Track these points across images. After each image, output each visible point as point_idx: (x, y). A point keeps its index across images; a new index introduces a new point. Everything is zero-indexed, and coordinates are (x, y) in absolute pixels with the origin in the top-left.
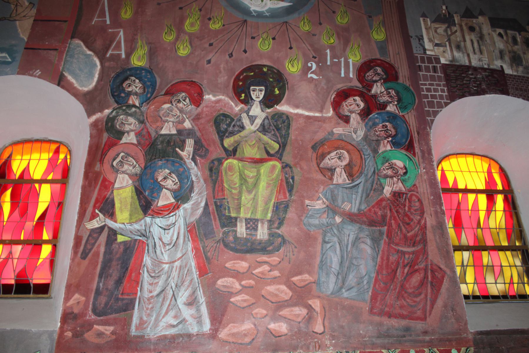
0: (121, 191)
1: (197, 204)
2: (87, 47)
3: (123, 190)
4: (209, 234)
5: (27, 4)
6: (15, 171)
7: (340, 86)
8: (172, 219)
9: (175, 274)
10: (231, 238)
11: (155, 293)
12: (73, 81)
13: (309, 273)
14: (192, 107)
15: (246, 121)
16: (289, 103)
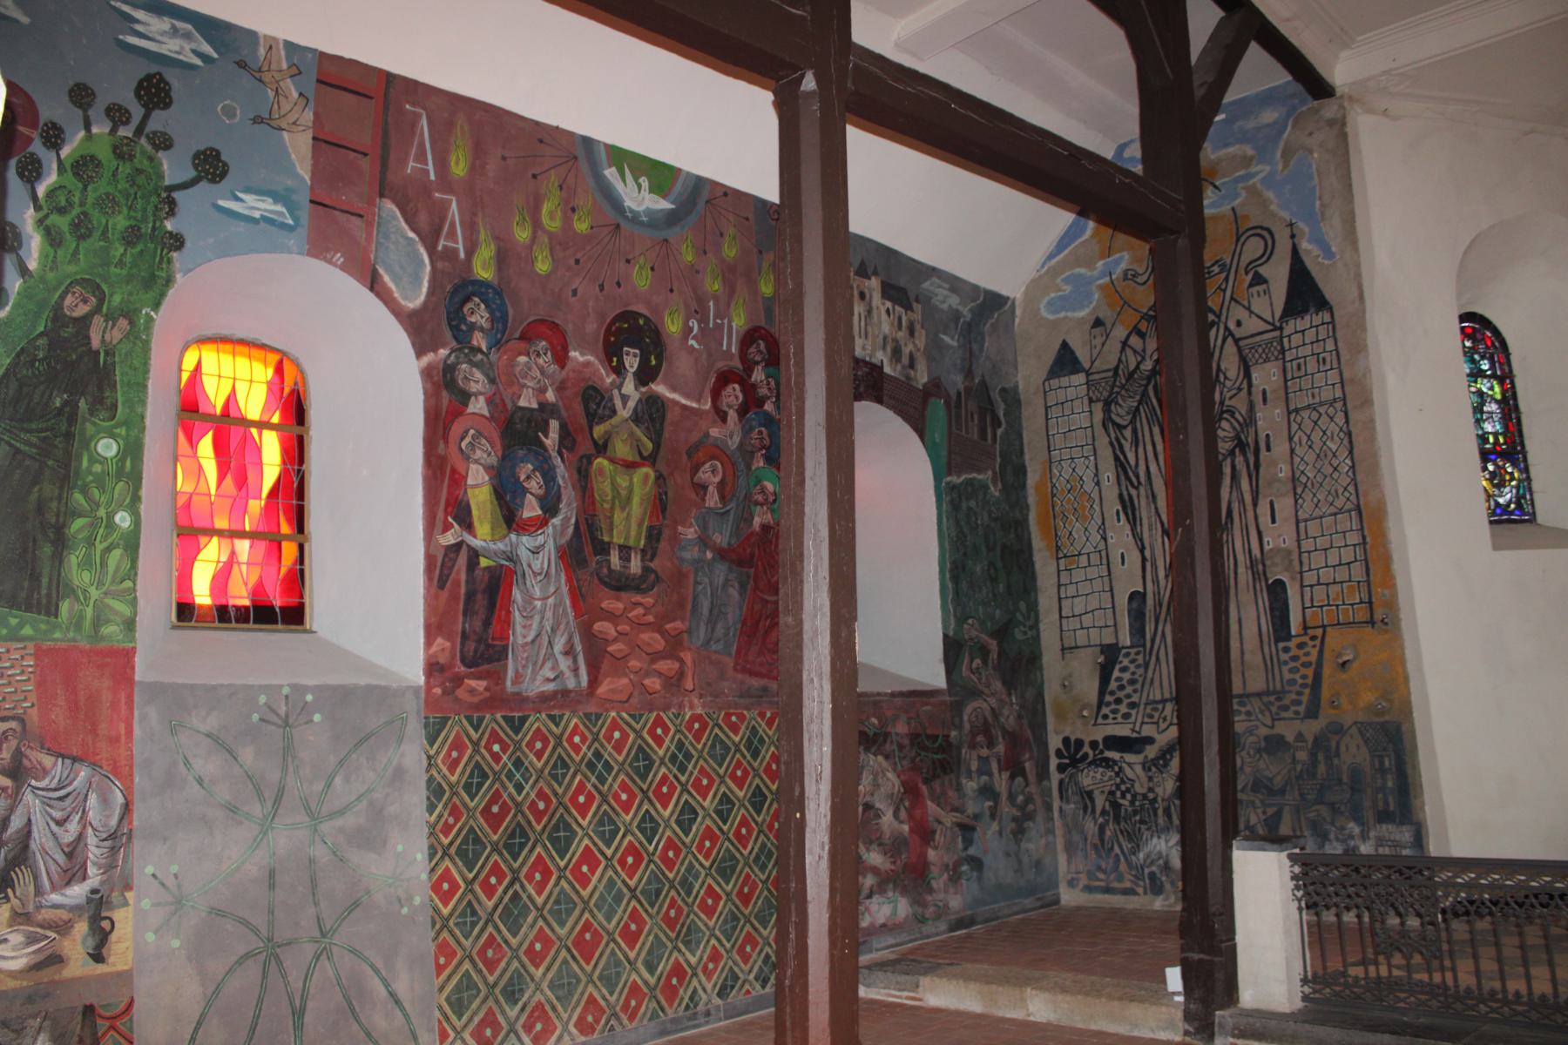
0: (477, 491)
1: (567, 519)
2: (407, 221)
3: (480, 494)
4: (582, 563)
5: (295, 95)
6: (212, 398)
7: (720, 365)
8: (541, 539)
9: (549, 614)
10: (605, 570)
11: (529, 639)
12: (391, 285)
13: (683, 620)
14: (554, 367)
15: (618, 402)
16: (665, 383)
